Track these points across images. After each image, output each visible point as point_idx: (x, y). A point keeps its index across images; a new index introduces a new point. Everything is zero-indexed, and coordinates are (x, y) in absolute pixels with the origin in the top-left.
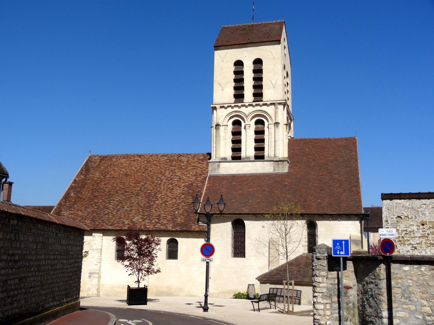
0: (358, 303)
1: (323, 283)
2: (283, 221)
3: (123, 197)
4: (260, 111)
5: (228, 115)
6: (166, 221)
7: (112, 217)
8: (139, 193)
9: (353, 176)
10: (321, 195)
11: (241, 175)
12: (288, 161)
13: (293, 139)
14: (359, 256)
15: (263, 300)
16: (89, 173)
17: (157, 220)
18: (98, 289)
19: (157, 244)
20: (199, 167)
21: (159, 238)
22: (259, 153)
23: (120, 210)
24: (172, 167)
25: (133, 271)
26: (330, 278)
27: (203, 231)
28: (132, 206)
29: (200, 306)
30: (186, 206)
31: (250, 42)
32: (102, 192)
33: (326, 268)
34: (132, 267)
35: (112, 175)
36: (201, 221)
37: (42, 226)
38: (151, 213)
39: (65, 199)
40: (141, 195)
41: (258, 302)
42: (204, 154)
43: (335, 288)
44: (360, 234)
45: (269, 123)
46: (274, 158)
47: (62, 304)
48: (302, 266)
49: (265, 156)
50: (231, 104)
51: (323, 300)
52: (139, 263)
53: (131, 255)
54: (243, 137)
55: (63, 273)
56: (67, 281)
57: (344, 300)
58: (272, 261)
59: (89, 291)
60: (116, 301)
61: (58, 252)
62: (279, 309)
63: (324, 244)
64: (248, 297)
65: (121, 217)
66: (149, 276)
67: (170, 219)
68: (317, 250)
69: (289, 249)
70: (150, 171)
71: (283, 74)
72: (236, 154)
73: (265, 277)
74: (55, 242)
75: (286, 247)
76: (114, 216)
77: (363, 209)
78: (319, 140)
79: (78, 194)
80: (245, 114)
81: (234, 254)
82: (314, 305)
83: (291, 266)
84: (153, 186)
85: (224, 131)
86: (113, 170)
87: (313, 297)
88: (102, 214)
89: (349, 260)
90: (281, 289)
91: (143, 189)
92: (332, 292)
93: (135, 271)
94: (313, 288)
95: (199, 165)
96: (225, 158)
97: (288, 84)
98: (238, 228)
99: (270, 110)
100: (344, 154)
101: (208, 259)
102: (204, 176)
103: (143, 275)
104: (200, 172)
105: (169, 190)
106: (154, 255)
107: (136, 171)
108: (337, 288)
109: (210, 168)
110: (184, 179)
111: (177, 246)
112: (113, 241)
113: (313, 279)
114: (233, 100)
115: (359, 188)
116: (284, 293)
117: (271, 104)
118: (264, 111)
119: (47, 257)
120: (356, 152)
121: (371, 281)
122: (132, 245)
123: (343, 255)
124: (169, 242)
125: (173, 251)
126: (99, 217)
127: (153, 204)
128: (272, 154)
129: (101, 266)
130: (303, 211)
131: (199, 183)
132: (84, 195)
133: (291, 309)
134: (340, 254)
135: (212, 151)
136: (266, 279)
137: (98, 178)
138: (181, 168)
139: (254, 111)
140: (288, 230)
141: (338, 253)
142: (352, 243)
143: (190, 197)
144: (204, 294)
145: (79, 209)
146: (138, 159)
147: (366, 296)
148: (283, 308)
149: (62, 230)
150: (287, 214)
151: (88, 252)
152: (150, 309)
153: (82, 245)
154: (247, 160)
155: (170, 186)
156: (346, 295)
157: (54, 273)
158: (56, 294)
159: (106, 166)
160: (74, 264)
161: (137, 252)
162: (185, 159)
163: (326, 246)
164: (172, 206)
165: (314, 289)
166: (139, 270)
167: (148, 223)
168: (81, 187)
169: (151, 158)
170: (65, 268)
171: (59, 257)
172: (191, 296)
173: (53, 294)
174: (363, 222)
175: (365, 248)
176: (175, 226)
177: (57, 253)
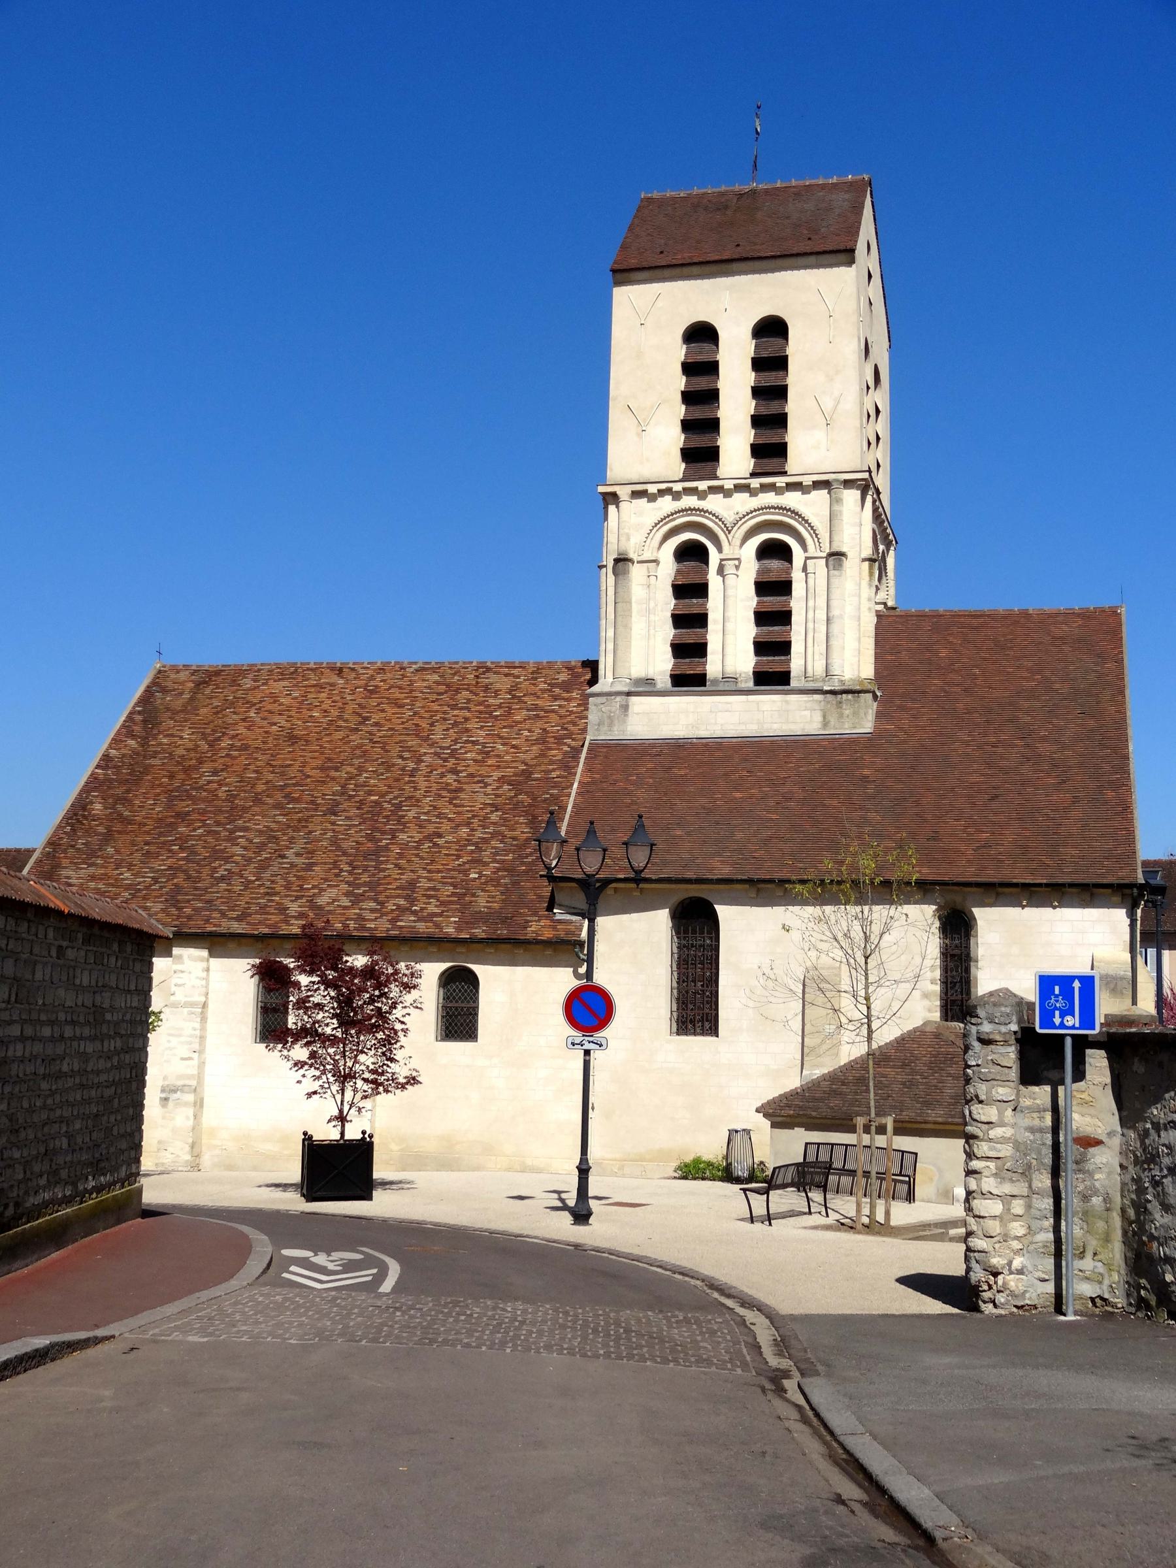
0: (1122, 1196)
1: (1002, 1124)
2: (858, 909)
3: (280, 818)
4: (775, 508)
5: (659, 522)
6: (436, 906)
7: (240, 890)
8: (338, 804)
10: (992, 817)
11: (704, 741)
12: (874, 693)
13: (892, 613)
14: (1130, 1033)
15: (784, 1186)
16: (155, 732)
17: (402, 902)
18: (193, 1146)
19: (408, 987)
20: (553, 711)
21: (413, 964)
22: (773, 661)
23: (270, 866)
24: (456, 712)
25: (320, 1082)
26: (1028, 1108)
27: (570, 941)
28: (315, 851)
29: (560, 1204)
31: (744, 255)
32: (204, 800)
33: (1014, 1074)
34: (318, 1069)
35: (239, 737)
36: (560, 906)
37: (11, 922)
38: (382, 875)
39: (72, 825)
40: (344, 810)
41: (766, 1192)
42: (573, 664)
43: (1044, 1144)
44: (1128, 956)
45: (807, 555)
46: (824, 681)
47: (82, 1196)
48: (920, 1067)
49: (792, 675)
50: (670, 485)
51: (1001, 1183)
52: (344, 1051)
53: (314, 1023)
54: (714, 605)
55: (82, 1086)
56: (97, 1116)
57: (1072, 1183)
58: (813, 1049)
59: (163, 1153)
60: (260, 1186)
61: (66, 1012)
62: (838, 1217)
63: (1007, 989)
64: (728, 1175)
66: (374, 1101)
67: (448, 896)
68: (981, 1012)
69: (876, 1007)
70: (376, 724)
71: (861, 374)
72: (689, 667)
74: (55, 980)
75: (867, 998)
76: (247, 884)
77: (1139, 865)
78: (989, 616)
79: (119, 807)
81: (677, 1022)
82: (967, 1200)
84: (387, 778)
85: (644, 580)
86: (244, 720)
87: (966, 1176)
88: (204, 880)
89: (1096, 1044)
90: (847, 1146)
91: (354, 790)
92: (1032, 1158)
93: (332, 1079)
94: (967, 1142)
96: (649, 681)
97: (878, 411)
99: (813, 506)
101: (591, 1039)
102: (573, 743)
103: (359, 1095)
104: (558, 730)
105: (444, 793)
106: (398, 1026)
107: (325, 725)
108: (1049, 1142)
109: (593, 716)
110: (498, 756)
111: (474, 995)
112: (252, 977)
113: (967, 1113)
116: (857, 1162)
117: (817, 485)
119: (29, 1031)
120: (1120, 662)
121: (1170, 1119)
122: (318, 989)
123: (1073, 1027)
124: (448, 980)
125: (453, 1013)
126: (196, 889)
127: (388, 844)
128: (818, 668)
129: (204, 1063)
130: (927, 873)
131: (554, 770)
133: (880, 1217)
134: (1062, 1026)
135: (602, 654)
136: (792, 1112)
137: (188, 750)
138: (487, 714)
139: (755, 510)
140: (874, 938)
141: (1057, 1020)
143: (522, 820)
145: (122, 860)
146: (332, 681)
147: (1150, 1170)
148: (852, 1213)
149: (80, 936)
150: (872, 883)
151: (160, 1013)
152: (387, 1216)
153: (146, 988)
155: (450, 779)
156: (1080, 1167)
157: (54, 1087)
158: (62, 1162)
160: (122, 1056)
161: (334, 1016)
163: (1015, 996)
164: (457, 850)
165: (970, 1146)
166: (344, 1078)
167: (372, 911)
168: (127, 780)
170: (89, 1069)
171: (68, 1032)
172: (524, 1169)
173: (51, 1160)
174: (1139, 912)
175: (1147, 1005)
176: (467, 923)
177: (62, 1016)
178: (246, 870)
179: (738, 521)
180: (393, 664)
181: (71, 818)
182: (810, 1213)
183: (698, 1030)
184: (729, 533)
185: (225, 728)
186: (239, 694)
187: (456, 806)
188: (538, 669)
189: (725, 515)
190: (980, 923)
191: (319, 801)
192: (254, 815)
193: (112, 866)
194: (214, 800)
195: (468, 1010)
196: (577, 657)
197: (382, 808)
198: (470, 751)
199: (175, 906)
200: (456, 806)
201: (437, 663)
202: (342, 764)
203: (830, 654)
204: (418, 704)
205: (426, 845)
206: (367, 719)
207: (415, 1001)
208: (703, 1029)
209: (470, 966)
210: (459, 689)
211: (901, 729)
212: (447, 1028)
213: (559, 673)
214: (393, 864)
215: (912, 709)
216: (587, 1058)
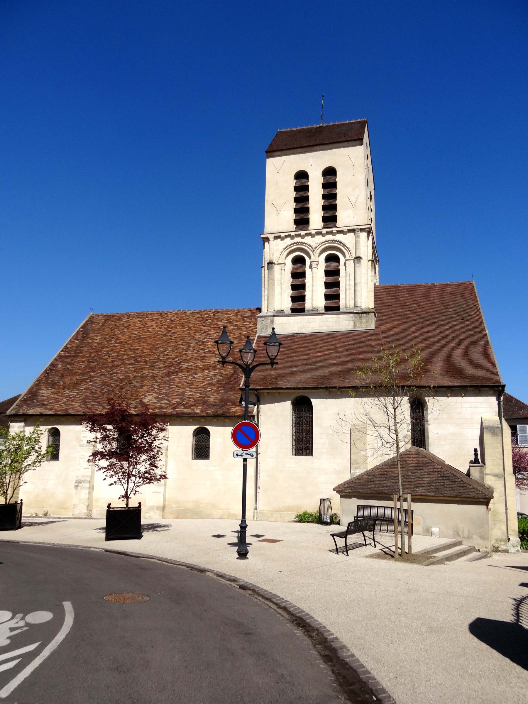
3: (132, 369)
5: (286, 248)
6: (193, 402)
9: (477, 332)
11: (305, 334)
16: (86, 338)
17: (178, 400)
18: (88, 506)
20: (244, 326)
23: (125, 387)
24: (205, 328)
30: (223, 380)
35: (119, 339)
38: (171, 390)
40: (158, 365)
42: (252, 309)
44: (498, 418)
45: (346, 259)
49: (340, 307)
54: (308, 281)
67: (198, 398)
70: (174, 333)
73: (348, 487)
75: (396, 431)
78: (419, 286)
79: (68, 366)
80: (310, 246)
84: (176, 353)
85: (279, 271)
86: (122, 333)
90: (378, 507)
91: (162, 357)
95: (245, 324)
96: (282, 311)
99: (348, 239)
100: (457, 304)
101: (247, 452)
105: (199, 358)
107: (153, 334)
109: (259, 326)
114: (292, 227)
115: (490, 348)
117: (350, 231)
118: (338, 241)
126: (94, 397)
127: (174, 378)
128: (351, 304)
132: (76, 367)
136: (350, 490)
137: (98, 344)
139: (324, 242)
142: (486, 432)
143: (230, 367)
144: (239, 522)
146: (157, 318)
154: (314, 313)
155: (201, 352)
159: (112, 328)
162: (224, 317)
164: (202, 379)
167: (166, 404)
174: (502, 398)
176: (205, 409)
178: (115, 389)
180: (181, 311)
182: (366, 545)
183: (304, 453)
184: (314, 251)
185: (114, 336)
187: (203, 362)
188: (238, 311)
193: (62, 388)
194: (106, 362)
195: (206, 446)
196: (253, 307)
197: (173, 364)
198: (210, 342)
199: (84, 404)
200: (203, 362)
202: (159, 348)
203: (356, 297)
204: (190, 325)
205: (190, 378)
206: (170, 331)
207: (164, 437)
208: (306, 453)
209: (206, 427)
210: (207, 319)
211: (387, 327)
212: (197, 454)
213: (246, 313)
214: (176, 385)
215: (390, 320)
216: (245, 463)
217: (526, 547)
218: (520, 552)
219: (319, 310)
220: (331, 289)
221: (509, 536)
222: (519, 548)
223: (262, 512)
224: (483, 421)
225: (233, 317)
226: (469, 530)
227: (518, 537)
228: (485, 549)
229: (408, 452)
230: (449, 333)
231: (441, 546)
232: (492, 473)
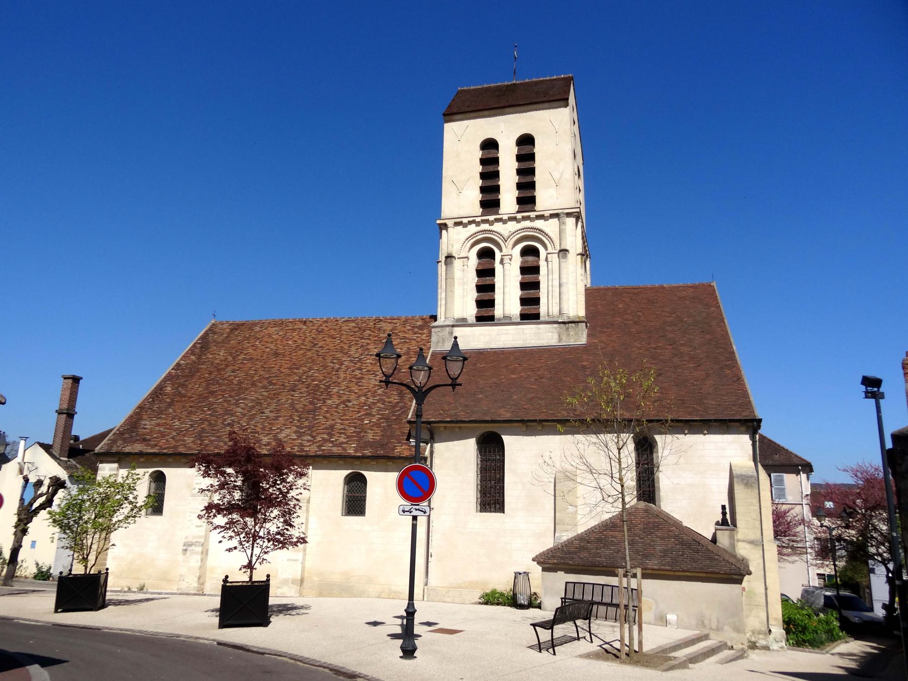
3: (264, 393)
4: (530, 228)
5: (469, 237)
6: (344, 438)
8: (296, 385)
11: (494, 350)
16: (206, 352)
17: (325, 436)
18: (199, 578)
20: (413, 339)
24: (363, 341)
28: (280, 410)
32: (225, 385)
35: (249, 354)
39: (153, 398)
40: (299, 389)
42: (425, 317)
44: (752, 464)
45: (547, 252)
49: (541, 315)
60: (206, 611)
65: (256, 429)
67: (351, 433)
70: (321, 347)
72: (485, 312)
73: (553, 557)
75: (621, 479)
79: (180, 389)
80: (501, 235)
81: (480, 504)
83: (613, 531)
84: (324, 373)
85: (461, 268)
86: (252, 346)
91: (305, 379)
95: (415, 337)
96: (464, 320)
98: (490, 452)
99: (550, 227)
101: (417, 507)
105: (353, 380)
107: (294, 348)
109: (434, 339)
117: (553, 216)
124: (349, 480)
126: (213, 430)
128: (555, 311)
136: (556, 561)
137: (221, 361)
139: (520, 230)
142: (738, 483)
143: (394, 393)
146: (300, 327)
155: (357, 372)
164: (358, 409)
167: (308, 441)
169: (324, 325)
178: (242, 420)
179: (510, 236)
181: (153, 395)
184: (506, 241)
186: (252, 334)
187: (359, 386)
189: (504, 233)
190: (659, 444)
191: (286, 384)
192: (250, 392)
194: (231, 385)
196: (426, 315)
199: (200, 439)
200: (359, 386)
201: (354, 318)
202: (301, 366)
203: (561, 303)
205: (342, 406)
210: (365, 330)
211: (602, 342)
212: (348, 508)
214: (322, 416)
216: (415, 522)
217: (793, 643)
218: (786, 649)
219: (512, 318)
220: (529, 291)
221: (770, 626)
222: (784, 644)
223: (434, 590)
224: (732, 467)
225: (399, 327)
226: (717, 618)
227: (782, 628)
228: (741, 646)
229: (633, 510)
230: (684, 349)
231: (681, 642)
232: (746, 539)
